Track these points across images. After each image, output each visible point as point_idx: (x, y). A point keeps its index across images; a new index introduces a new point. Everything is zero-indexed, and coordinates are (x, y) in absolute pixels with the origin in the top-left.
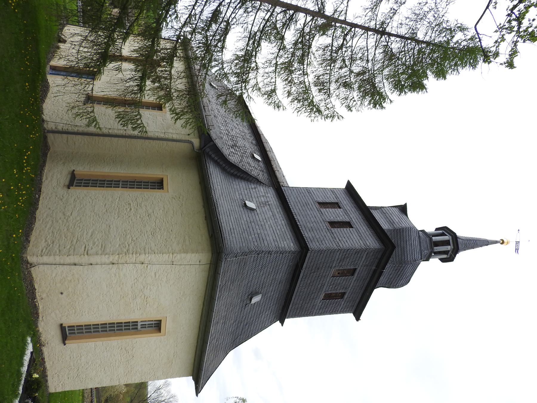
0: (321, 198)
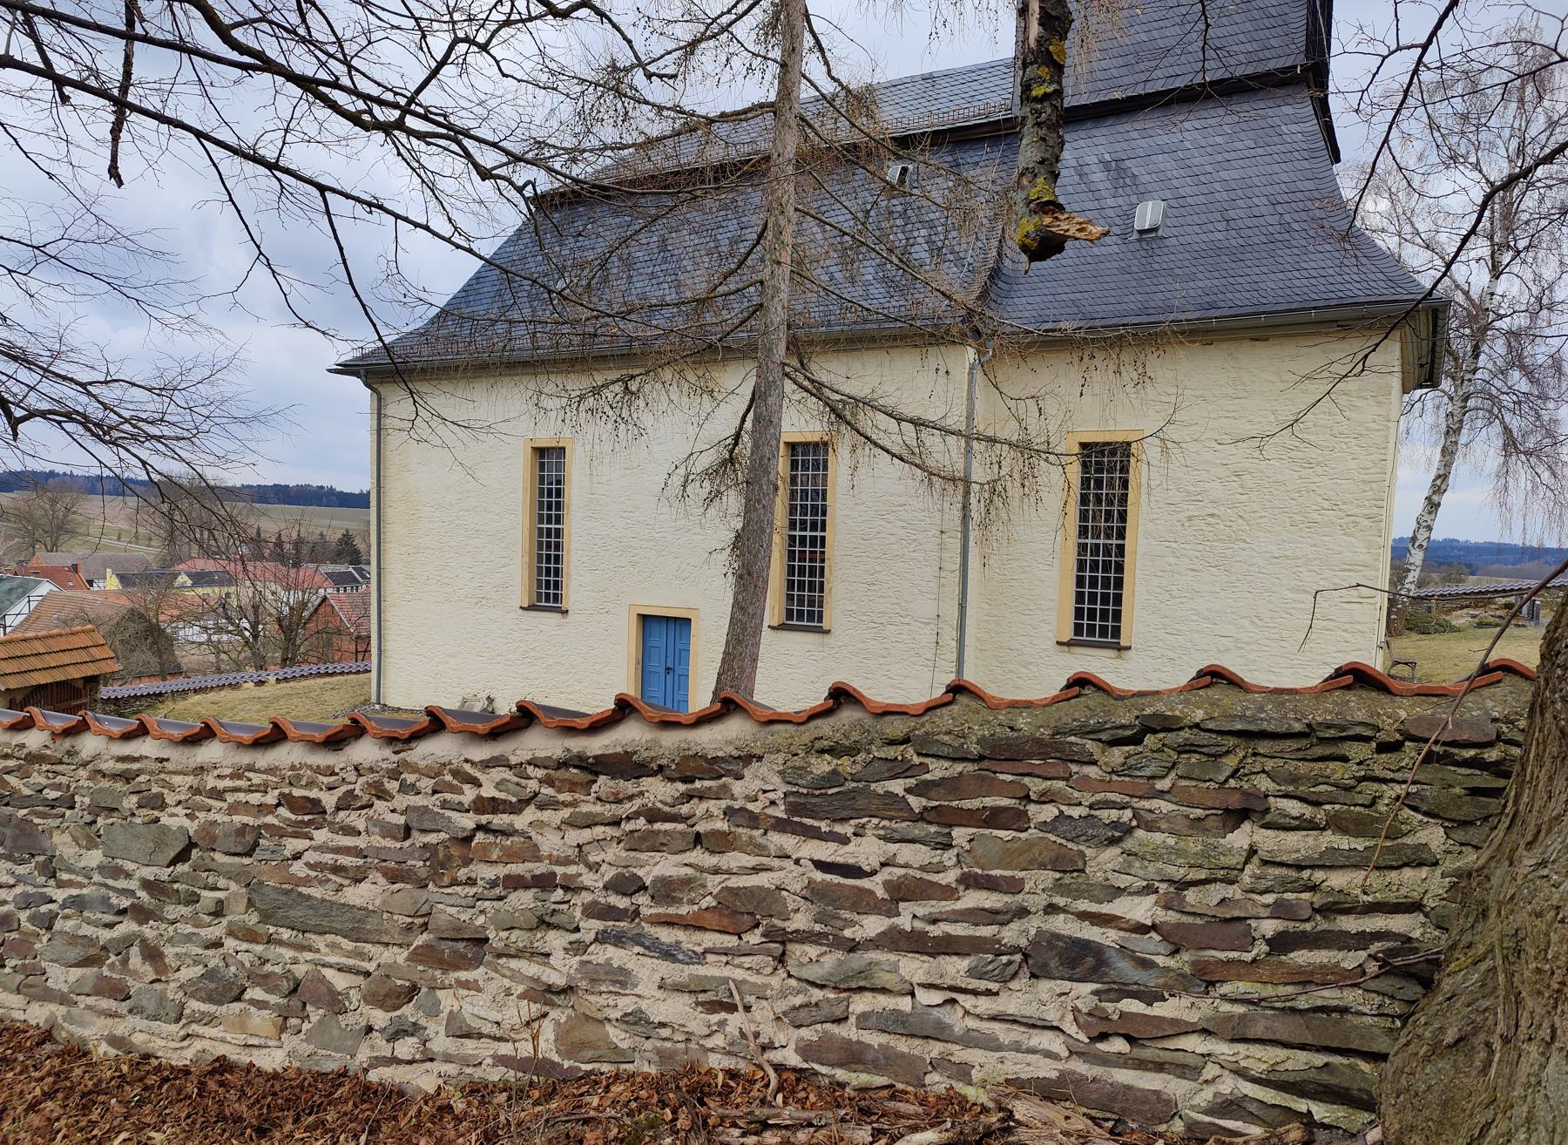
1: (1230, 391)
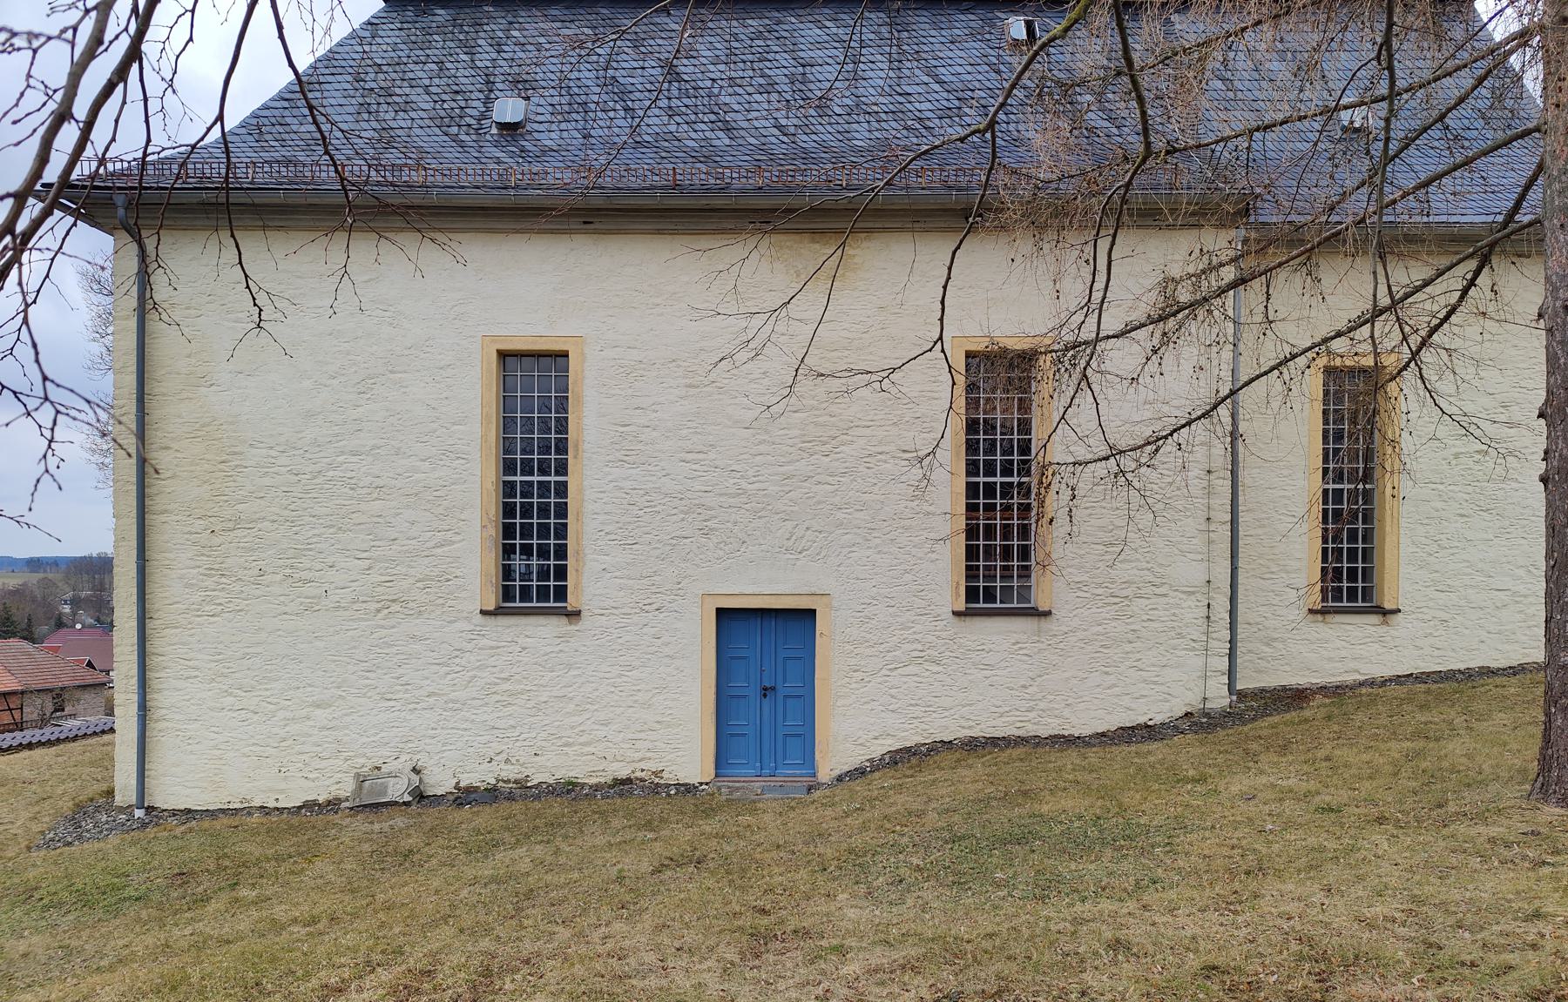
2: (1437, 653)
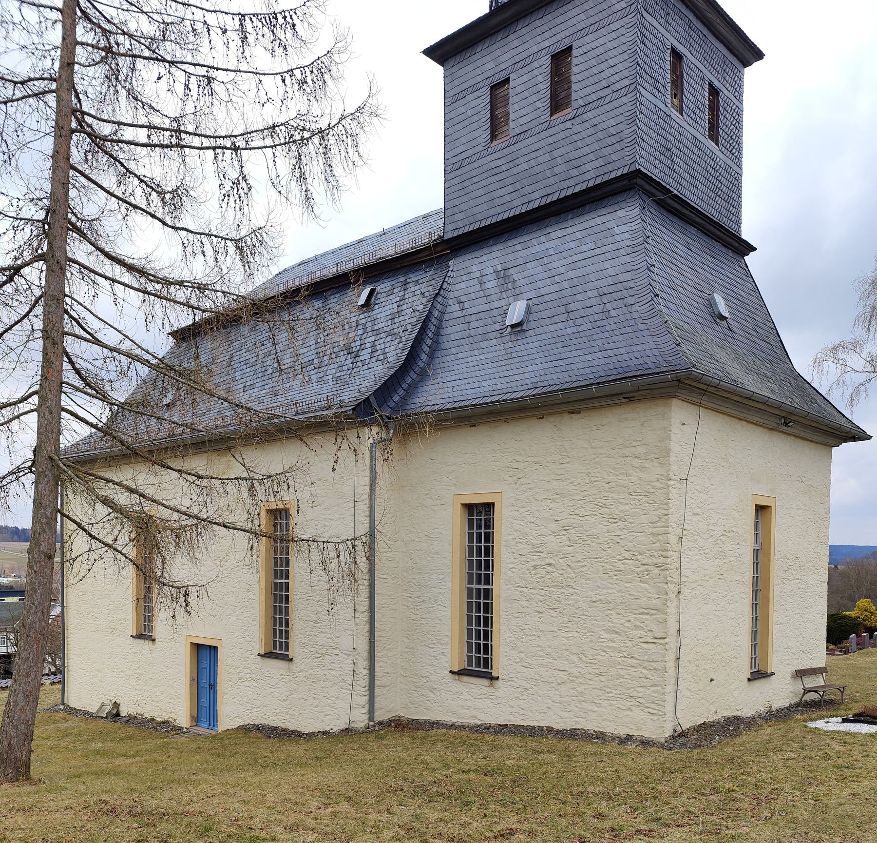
0: (476, 134)
1: (557, 457)
2: (522, 712)
